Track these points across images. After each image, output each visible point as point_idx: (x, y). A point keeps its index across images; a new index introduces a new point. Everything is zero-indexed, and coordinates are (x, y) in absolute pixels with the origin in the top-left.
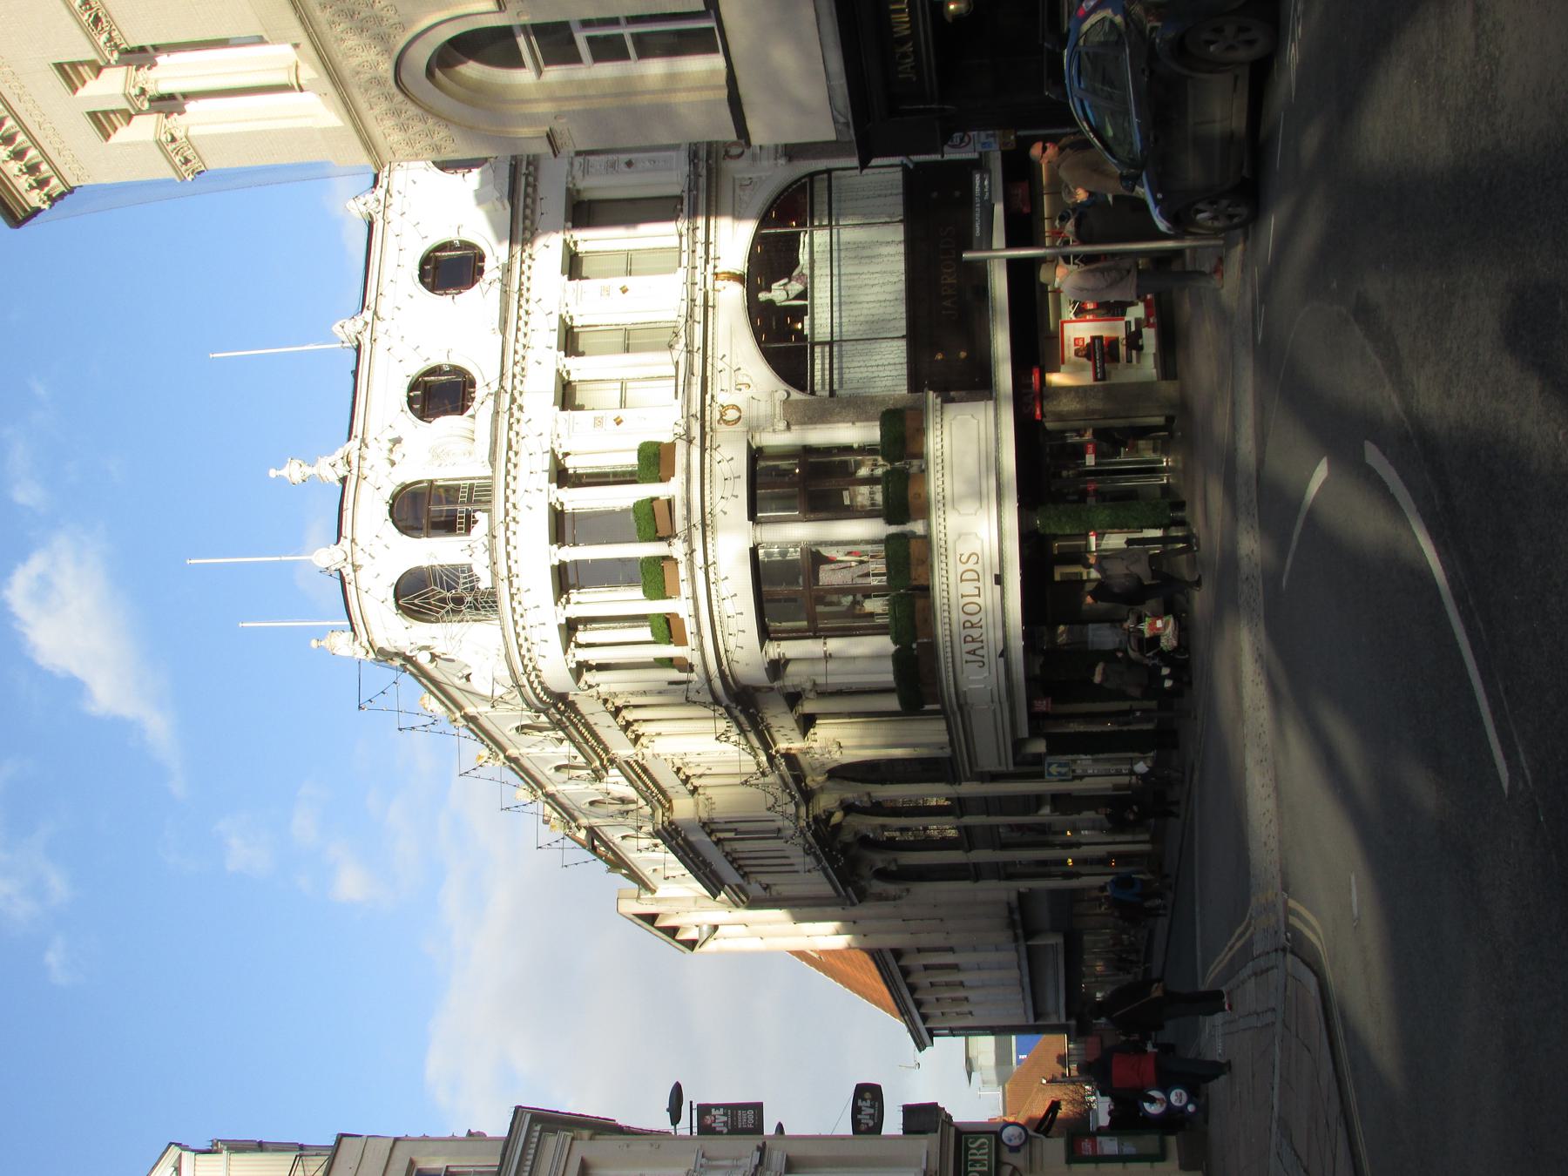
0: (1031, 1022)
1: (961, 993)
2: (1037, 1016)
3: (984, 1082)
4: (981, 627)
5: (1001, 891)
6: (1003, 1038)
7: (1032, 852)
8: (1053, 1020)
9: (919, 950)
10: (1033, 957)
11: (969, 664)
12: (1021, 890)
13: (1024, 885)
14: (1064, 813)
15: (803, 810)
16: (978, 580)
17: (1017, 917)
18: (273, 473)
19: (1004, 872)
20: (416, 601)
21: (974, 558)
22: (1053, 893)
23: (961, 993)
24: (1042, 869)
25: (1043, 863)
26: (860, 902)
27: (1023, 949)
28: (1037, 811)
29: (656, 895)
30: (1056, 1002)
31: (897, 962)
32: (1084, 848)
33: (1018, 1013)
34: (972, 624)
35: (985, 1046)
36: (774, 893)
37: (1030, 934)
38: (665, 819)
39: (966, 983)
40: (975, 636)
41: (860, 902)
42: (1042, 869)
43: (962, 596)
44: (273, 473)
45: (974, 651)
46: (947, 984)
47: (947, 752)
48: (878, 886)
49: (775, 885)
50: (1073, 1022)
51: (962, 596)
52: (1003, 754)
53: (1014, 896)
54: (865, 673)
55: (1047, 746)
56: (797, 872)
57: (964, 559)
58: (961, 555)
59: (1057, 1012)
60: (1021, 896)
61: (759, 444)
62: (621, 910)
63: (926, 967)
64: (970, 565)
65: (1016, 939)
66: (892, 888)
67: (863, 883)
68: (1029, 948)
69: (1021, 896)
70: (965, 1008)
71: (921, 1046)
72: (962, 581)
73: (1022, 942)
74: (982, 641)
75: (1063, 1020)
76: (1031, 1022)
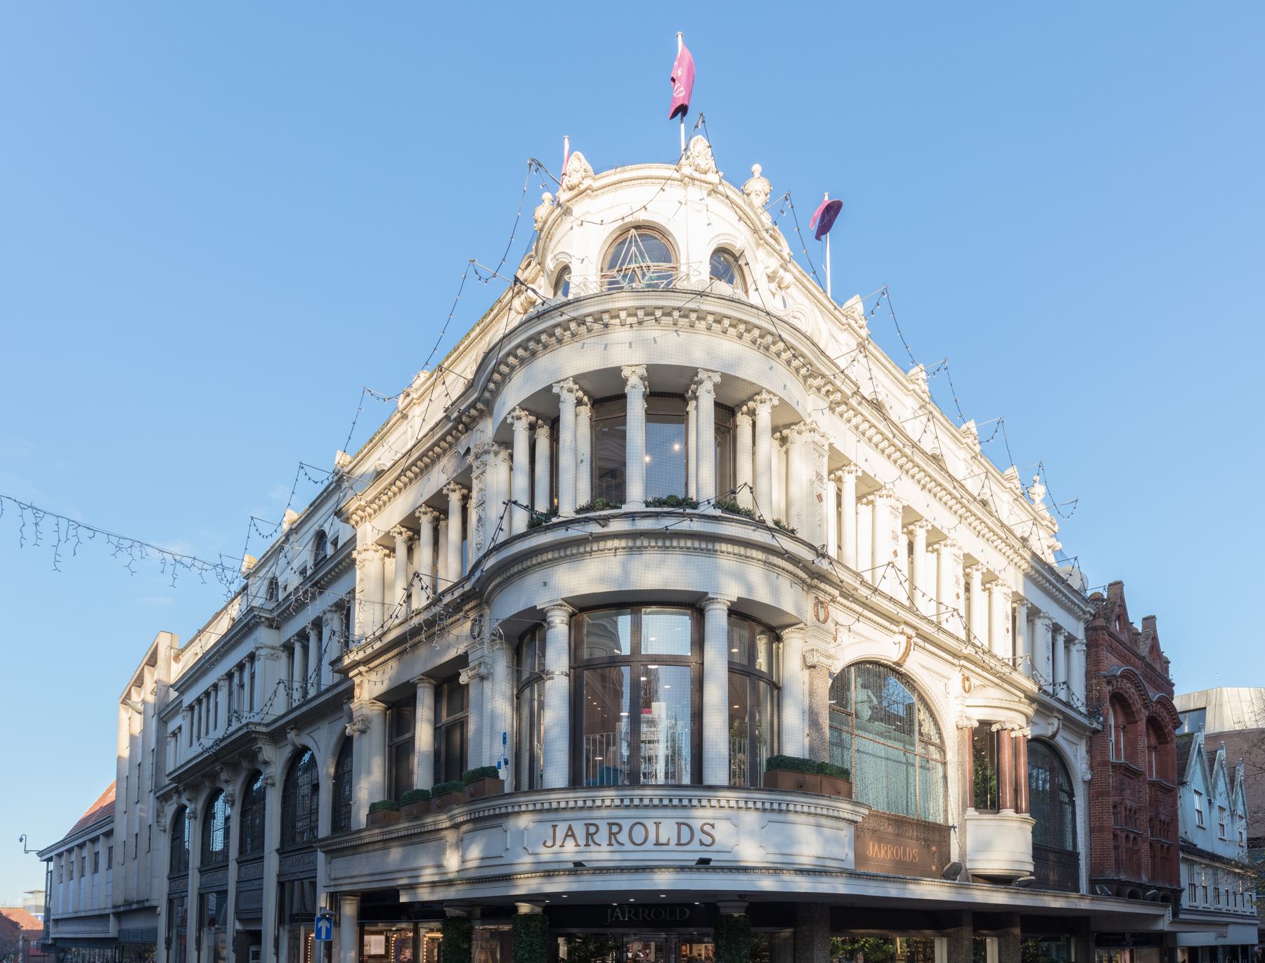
0: (52, 917)
1: (76, 875)
2: (56, 921)
3: (26, 899)
4: (587, 845)
5: (159, 894)
6: (43, 909)
7: (195, 917)
8: (52, 930)
9: (110, 848)
10: (103, 917)
11: (552, 829)
12: (159, 908)
13: (163, 909)
14: (234, 940)
15: (264, 729)
16: (679, 844)
17: (135, 906)
18: (757, 168)
19: (176, 899)
20: (633, 248)
21: (709, 840)
22: (154, 932)
23: (76, 875)
24: (177, 922)
25: (184, 921)
26: (157, 798)
27: (107, 911)
28: (239, 920)
29: (173, 662)
30: (67, 931)
31: (102, 834)
32: (196, 953)
33: (57, 913)
34: (592, 835)
35: (41, 900)
36: (169, 739)
37: (119, 915)
38: (263, 619)
39: (83, 879)
40: (596, 838)
41: (157, 798)
42: (177, 922)
43: (657, 824)
44: (757, 168)
45: (573, 836)
46: (83, 868)
47: (354, 828)
48: (170, 809)
49: (177, 741)
50: (50, 942)
51: (657, 824)
52: (357, 880)
53: (154, 903)
54: (77, 933)
55: (526, 914)
56: (191, 744)
57: (707, 828)
58: (713, 826)
59: (58, 933)
60: (154, 908)
61: (785, 637)
62: (161, 633)
63: (97, 854)
64: (698, 835)
65: (114, 907)
66: (167, 820)
67: (174, 797)
68: (109, 915)
69: (154, 908)
70: (65, 878)
71: (40, 854)
72: (679, 824)
73: (112, 911)
74: (587, 845)
75: (52, 936)
76: (52, 917)
